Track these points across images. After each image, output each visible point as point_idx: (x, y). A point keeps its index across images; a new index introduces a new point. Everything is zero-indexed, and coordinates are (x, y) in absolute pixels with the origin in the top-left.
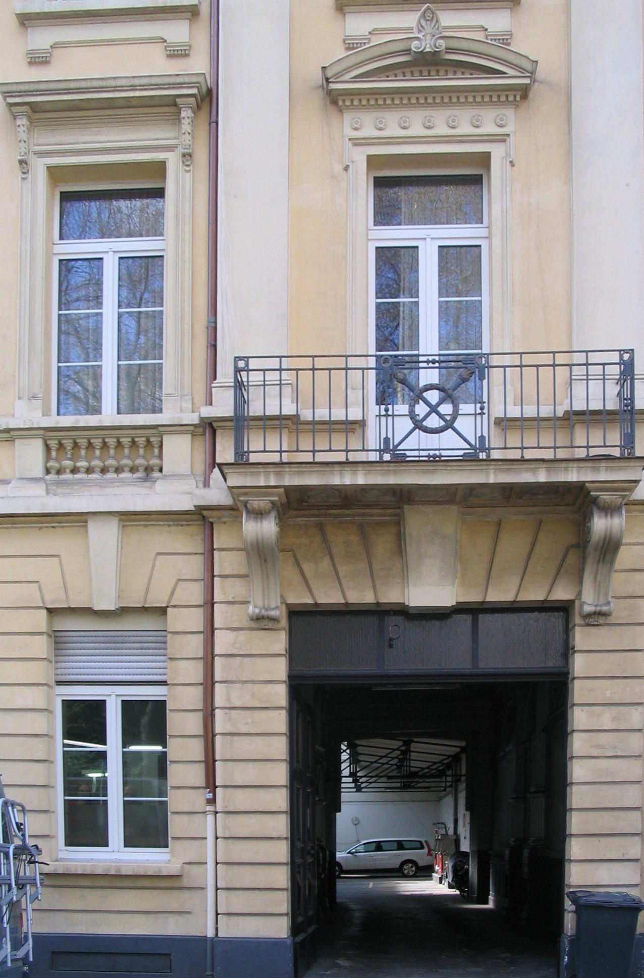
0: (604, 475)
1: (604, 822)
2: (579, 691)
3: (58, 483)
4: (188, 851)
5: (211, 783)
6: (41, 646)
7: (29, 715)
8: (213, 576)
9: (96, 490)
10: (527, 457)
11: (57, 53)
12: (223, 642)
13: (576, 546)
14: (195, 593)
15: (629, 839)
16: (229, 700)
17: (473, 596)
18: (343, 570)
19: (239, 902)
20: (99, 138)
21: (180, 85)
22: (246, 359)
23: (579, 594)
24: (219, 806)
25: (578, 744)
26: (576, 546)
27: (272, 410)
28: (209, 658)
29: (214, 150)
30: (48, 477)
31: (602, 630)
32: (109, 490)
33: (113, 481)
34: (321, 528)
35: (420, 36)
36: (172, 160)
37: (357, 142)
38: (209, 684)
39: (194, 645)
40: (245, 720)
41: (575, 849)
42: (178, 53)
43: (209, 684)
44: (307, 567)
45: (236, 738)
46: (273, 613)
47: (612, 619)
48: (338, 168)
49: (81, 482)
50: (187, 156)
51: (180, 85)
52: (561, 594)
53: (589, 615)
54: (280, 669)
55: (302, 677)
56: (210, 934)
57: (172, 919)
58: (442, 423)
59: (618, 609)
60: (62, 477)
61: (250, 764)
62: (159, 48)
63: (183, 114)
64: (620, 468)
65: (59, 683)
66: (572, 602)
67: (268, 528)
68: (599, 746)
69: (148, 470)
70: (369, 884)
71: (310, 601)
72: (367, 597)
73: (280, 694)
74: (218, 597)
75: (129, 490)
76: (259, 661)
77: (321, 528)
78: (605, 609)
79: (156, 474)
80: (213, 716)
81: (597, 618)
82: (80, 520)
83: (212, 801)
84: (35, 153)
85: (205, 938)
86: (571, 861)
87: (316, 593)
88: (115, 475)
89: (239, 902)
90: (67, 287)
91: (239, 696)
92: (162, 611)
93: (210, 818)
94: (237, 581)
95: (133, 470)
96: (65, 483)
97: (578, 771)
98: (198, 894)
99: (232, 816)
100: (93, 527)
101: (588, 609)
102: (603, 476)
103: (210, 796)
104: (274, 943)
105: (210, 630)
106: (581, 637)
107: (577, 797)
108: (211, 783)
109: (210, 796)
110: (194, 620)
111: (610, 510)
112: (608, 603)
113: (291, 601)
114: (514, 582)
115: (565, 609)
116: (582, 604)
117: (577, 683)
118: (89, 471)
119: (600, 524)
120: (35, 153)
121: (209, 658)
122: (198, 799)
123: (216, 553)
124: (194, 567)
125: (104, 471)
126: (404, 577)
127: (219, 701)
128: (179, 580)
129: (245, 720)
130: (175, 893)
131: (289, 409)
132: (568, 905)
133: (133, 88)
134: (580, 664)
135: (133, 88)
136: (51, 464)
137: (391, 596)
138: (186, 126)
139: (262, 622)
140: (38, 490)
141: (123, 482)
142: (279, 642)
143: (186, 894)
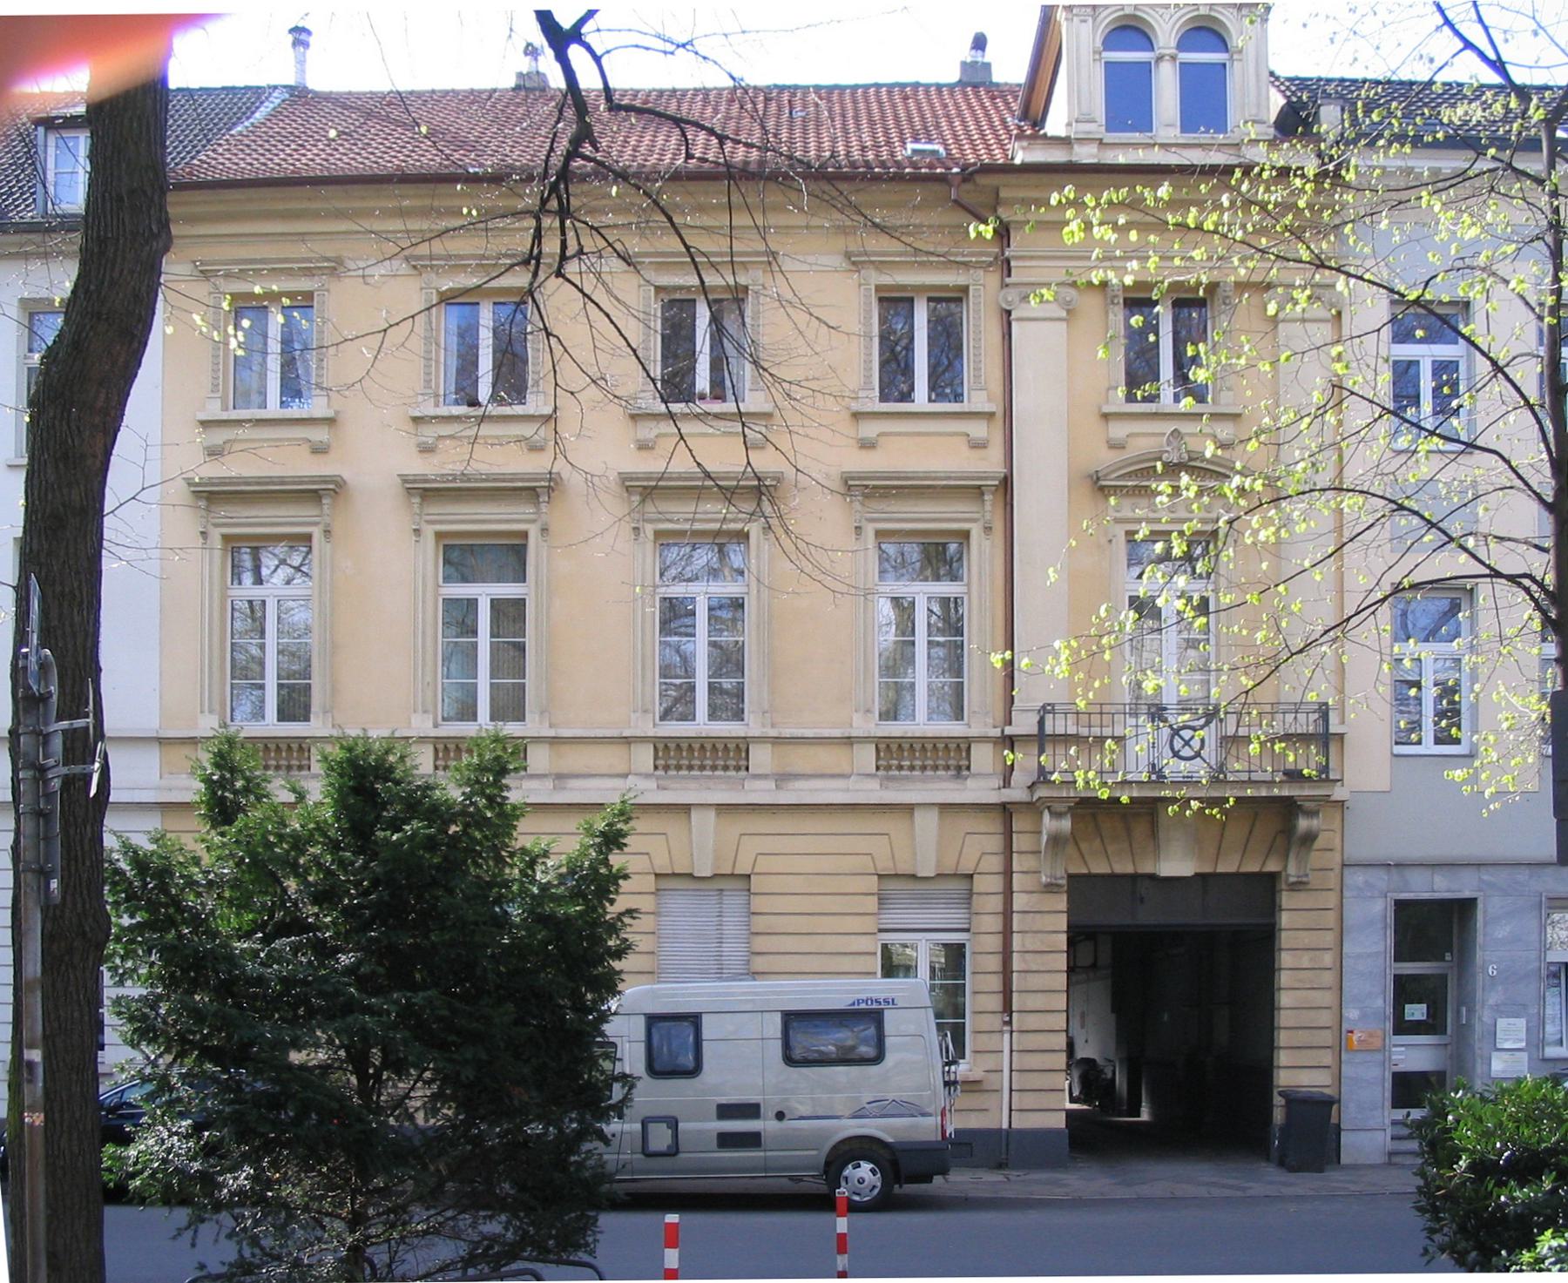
0: (1307, 791)
1: (1303, 1038)
2: (1285, 939)
3: (889, 778)
4: (989, 1062)
5: (1007, 1008)
6: (871, 904)
7: (862, 958)
8: (1012, 852)
9: (919, 785)
10: (1253, 778)
11: (882, 440)
12: (1019, 902)
13: (1282, 832)
14: (995, 863)
15: (1323, 1051)
16: (1023, 945)
17: (1207, 869)
18: (1110, 849)
19: (1029, 1101)
20: (916, 509)
21: (986, 478)
22: (1053, 705)
23: (1285, 867)
24: (1015, 1026)
25: (1284, 979)
26: (1282, 832)
27: (1060, 730)
28: (1007, 913)
29: (1009, 525)
30: (879, 773)
31: (1302, 895)
32: (930, 786)
33: (932, 778)
34: (1094, 816)
35: (1168, 449)
36: (976, 531)
37: (1117, 521)
38: (1007, 933)
39: (996, 903)
40: (1035, 962)
41: (1283, 1058)
42: (978, 445)
43: (1007, 933)
44: (1083, 846)
45: (1028, 975)
46: (1060, 882)
47: (1309, 887)
48: (1104, 541)
49: (906, 778)
50: (988, 529)
51: (986, 478)
52: (1272, 866)
53: (1293, 884)
54: (1062, 922)
55: (1077, 927)
56: (1005, 1126)
57: (973, 1115)
58: (1181, 733)
59: (1314, 879)
60: (891, 773)
61: (1039, 995)
62: (964, 439)
63: (986, 497)
64: (1319, 787)
65: (881, 931)
66: (1279, 873)
67: (1066, 824)
68: (1300, 981)
69: (959, 768)
70: (31, 1125)
71: (1084, 871)
72: (1129, 869)
73: (1062, 941)
74: (1015, 867)
75: (945, 785)
76: (1047, 916)
77: (1094, 816)
78: (1305, 879)
79: (965, 773)
80: (1011, 958)
81: (1298, 886)
82: (909, 809)
83: (1010, 1023)
84: (866, 519)
85: (1000, 1130)
86: (1279, 1067)
87: (1090, 866)
88: (932, 773)
89: (1029, 1101)
90: (506, 256)
91: (1032, 943)
92: (971, 876)
93: (1007, 1036)
94: (1030, 856)
95: (947, 768)
96: (893, 778)
97: (1285, 999)
98: (994, 1095)
99: (1025, 1035)
100: (919, 815)
101: (1292, 879)
102: (1306, 792)
103: (1007, 1019)
104: (1056, 1132)
105: (1008, 893)
106: (1286, 899)
107: (1284, 1018)
108: (1007, 1008)
109: (1007, 1019)
110: (996, 883)
111: (1312, 814)
112: (1307, 875)
113: (1070, 872)
114: (1237, 857)
115: (1273, 877)
116: (1288, 876)
117: (1284, 934)
118: (912, 768)
119: (1303, 824)
120: (866, 519)
121: (1007, 913)
122: (995, 1022)
123: (1014, 836)
124: (995, 843)
125: (924, 768)
126: (1157, 858)
127: (1016, 947)
128: (983, 853)
129: (1035, 962)
130: (977, 1094)
131: (1072, 730)
132: (1278, 1100)
133: (949, 478)
134: (1285, 919)
135: (949, 478)
136: (881, 762)
137: (1146, 868)
138: (988, 507)
139: (1050, 888)
140: (874, 784)
141: (940, 778)
142: (1061, 902)
143: (986, 1095)
